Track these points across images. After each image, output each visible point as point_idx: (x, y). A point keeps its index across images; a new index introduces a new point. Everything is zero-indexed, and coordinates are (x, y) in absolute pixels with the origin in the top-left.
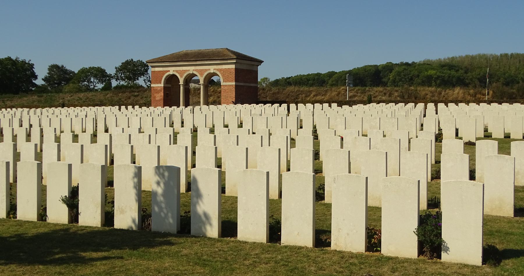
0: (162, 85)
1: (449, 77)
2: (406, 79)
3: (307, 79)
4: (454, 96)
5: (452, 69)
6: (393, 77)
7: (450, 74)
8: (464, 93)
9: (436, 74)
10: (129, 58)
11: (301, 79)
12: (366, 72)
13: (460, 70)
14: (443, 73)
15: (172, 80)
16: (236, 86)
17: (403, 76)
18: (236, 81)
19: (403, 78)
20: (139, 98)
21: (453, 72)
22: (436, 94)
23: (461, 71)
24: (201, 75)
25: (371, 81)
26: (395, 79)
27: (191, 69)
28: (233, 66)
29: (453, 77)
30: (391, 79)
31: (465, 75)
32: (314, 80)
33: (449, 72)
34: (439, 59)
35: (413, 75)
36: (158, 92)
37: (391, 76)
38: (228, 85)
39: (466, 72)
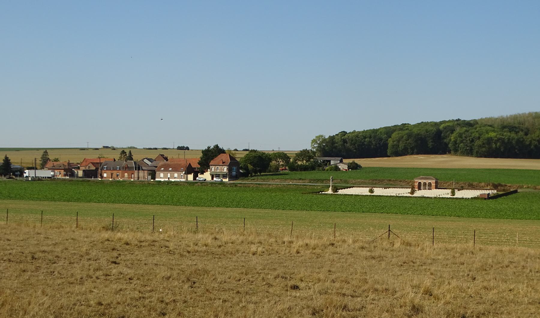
5: (513, 130)
6: (454, 138)
7: (510, 136)
9: (496, 137)
10: (305, 149)
13: (521, 132)
14: (503, 135)
15: (420, 183)
17: (464, 138)
19: (464, 140)
21: (513, 135)
23: (521, 133)
25: (432, 142)
26: (457, 140)
29: (513, 139)
31: (524, 137)
32: (370, 137)
33: (509, 134)
35: (474, 137)
37: (452, 137)
38: (433, 185)
39: (526, 134)
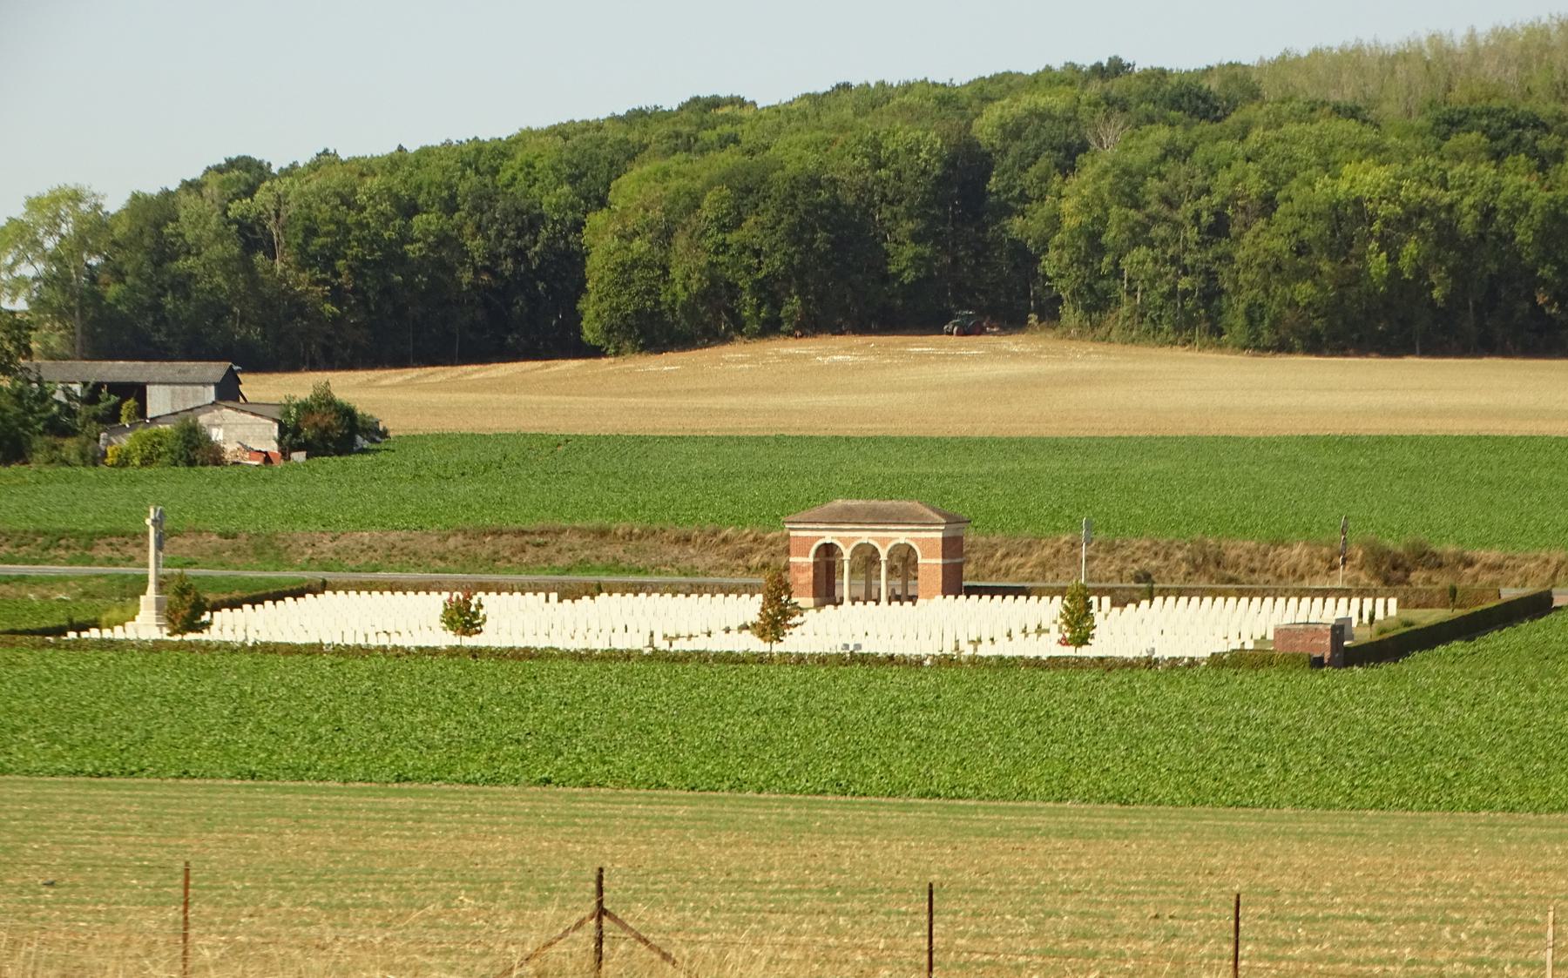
0: (811, 559)
1: (1488, 214)
2: (1177, 226)
3: (396, 199)
4: (1292, 561)
6: (1086, 206)
7: (1496, 190)
8: (1311, 555)
9: (1391, 195)
11: (347, 201)
12: (878, 165)
14: (1444, 184)
15: (828, 550)
16: (944, 565)
18: (944, 557)
19: (1154, 219)
20: (552, 550)
22: (1258, 557)
24: (884, 546)
26: (1103, 221)
27: (865, 537)
28: (940, 535)
30: (1070, 223)
33: (1487, 172)
34: (1434, 39)
35: (1231, 199)
36: (804, 570)
37: (1073, 199)
38: (931, 563)
